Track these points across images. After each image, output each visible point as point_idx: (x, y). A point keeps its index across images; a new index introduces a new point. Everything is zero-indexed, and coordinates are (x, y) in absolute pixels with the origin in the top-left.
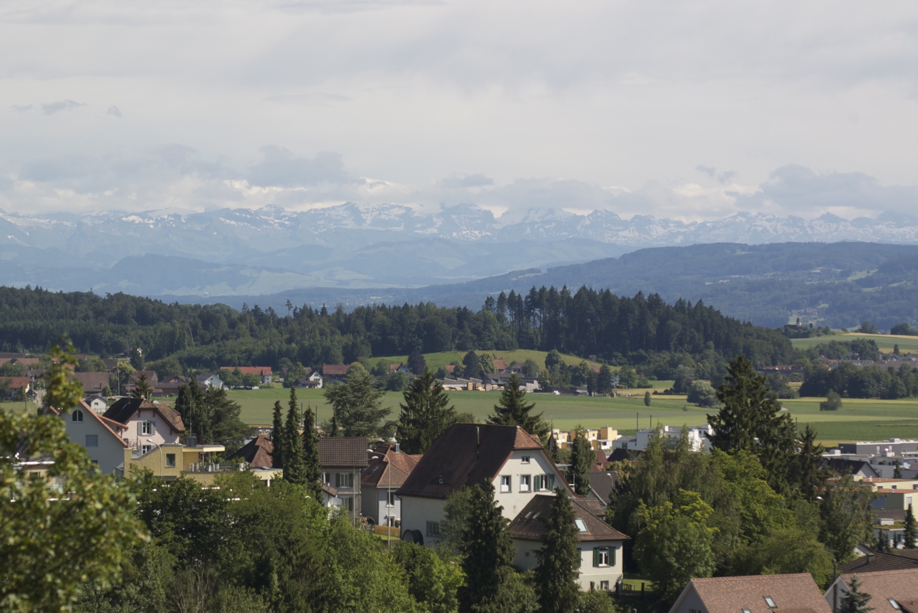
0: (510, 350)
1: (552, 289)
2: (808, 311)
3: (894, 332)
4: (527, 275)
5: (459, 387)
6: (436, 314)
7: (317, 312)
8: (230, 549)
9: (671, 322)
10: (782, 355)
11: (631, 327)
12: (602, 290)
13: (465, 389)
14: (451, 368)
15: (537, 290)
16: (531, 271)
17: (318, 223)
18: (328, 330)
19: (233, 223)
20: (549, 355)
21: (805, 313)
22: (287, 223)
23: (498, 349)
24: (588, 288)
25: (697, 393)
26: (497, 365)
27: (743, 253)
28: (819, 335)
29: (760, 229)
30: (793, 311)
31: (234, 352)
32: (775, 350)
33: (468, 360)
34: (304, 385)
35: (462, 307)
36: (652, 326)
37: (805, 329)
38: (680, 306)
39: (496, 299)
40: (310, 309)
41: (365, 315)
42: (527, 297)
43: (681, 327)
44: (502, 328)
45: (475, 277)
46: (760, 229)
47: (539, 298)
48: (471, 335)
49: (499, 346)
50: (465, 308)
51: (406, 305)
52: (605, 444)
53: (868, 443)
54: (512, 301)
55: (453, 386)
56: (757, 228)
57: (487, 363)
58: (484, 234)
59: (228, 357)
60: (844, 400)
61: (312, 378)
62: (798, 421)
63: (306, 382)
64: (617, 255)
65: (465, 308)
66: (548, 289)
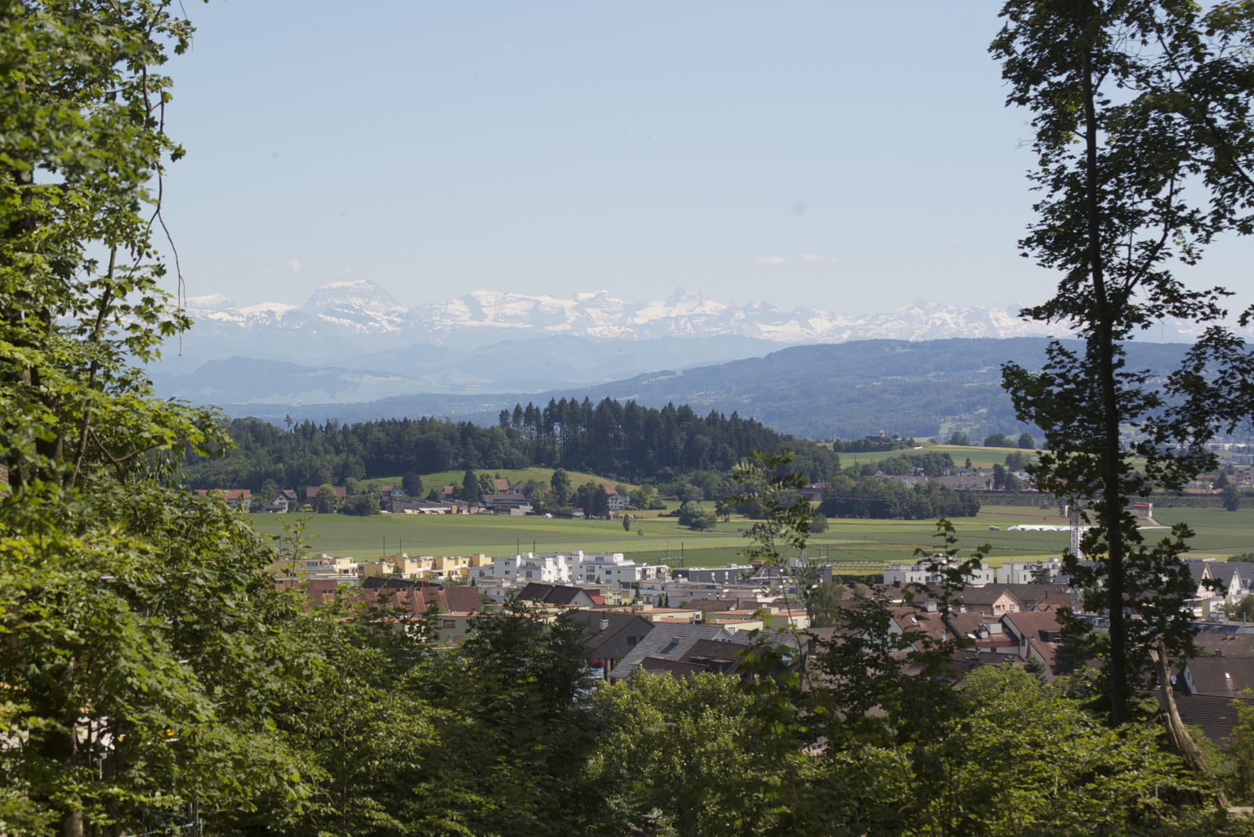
0: (520, 468)
1: (573, 402)
2: (963, 417)
3: (987, 443)
4: (660, 378)
5: (441, 510)
6: (439, 430)
7: (321, 427)
8: (384, 720)
9: (700, 436)
10: (823, 471)
11: (656, 443)
12: (553, 401)
13: (448, 512)
14: (449, 489)
15: (557, 402)
16: (665, 373)
17: (434, 318)
18: (321, 448)
19: (334, 319)
20: (555, 475)
21: (961, 419)
22: (396, 319)
23: (506, 468)
24: (612, 399)
25: (689, 515)
26: (499, 485)
27: (903, 351)
28: (902, 448)
29: (938, 322)
30: (947, 418)
31: (220, 474)
32: (815, 466)
33: (468, 480)
34: (268, 510)
35: (467, 422)
36: (679, 439)
37: (888, 441)
38: (713, 419)
39: (512, 413)
40: (313, 425)
41: (362, 432)
42: (546, 410)
43: (710, 442)
44: (511, 444)
45: (608, 380)
46: (938, 322)
47: (562, 411)
48: (476, 452)
49: (509, 464)
50: (470, 423)
51: (405, 420)
52: (441, 574)
53: (703, 569)
54: (530, 414)
55: (435, 509)
56: (936, 320)
57: (486, 484)
58: (623, 330)
59: (213, 478)
60: (830, 520)
61: (276, 503)
62: (685, 548)
63: (270, 507)
64: (762, 354)
65: (470, 423)
66: (568, 401)
